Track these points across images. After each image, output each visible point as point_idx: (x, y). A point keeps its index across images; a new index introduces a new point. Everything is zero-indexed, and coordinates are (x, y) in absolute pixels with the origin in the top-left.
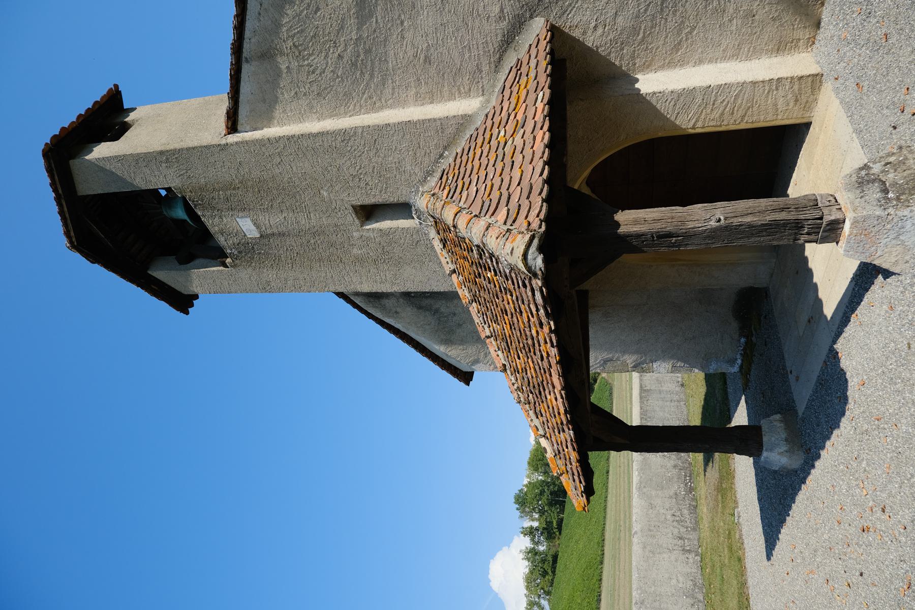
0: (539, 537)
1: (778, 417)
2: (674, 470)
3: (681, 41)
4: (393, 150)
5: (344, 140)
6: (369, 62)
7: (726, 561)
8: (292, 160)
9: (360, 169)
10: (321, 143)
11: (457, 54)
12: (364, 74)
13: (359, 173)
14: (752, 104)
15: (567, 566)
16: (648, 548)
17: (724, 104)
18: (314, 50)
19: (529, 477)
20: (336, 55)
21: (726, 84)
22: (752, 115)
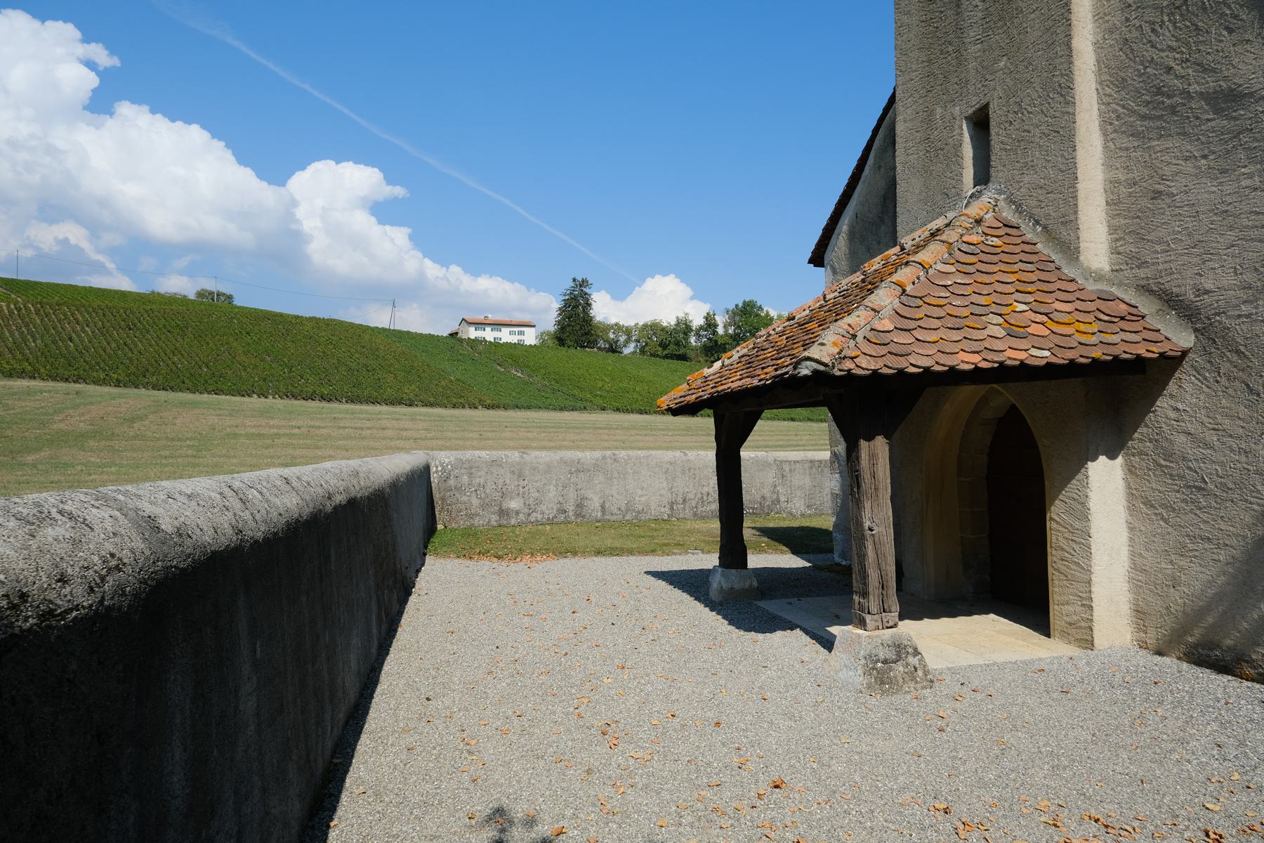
0: (706, 336)
1: (755, 584)
2: (759, 496)
3: (1155, 507)
4: (1047, 157)
5: (1061, 88)
6: (1159, 113)
7: (656, 541)
8: (1042, 11)
9: (1028, 112)
10: (1060, 54)
11: (1161, 234)
12: (1147, 106)
13: (1024, 110)
14: (1069, 580)
15: (675, 374)
16: (671, 468)
17: (1072, 552)
18: (1180, 29)
19: (780, 317)
20: (1172, 64)
21: (1091, 553)
22: (1059, 580)
